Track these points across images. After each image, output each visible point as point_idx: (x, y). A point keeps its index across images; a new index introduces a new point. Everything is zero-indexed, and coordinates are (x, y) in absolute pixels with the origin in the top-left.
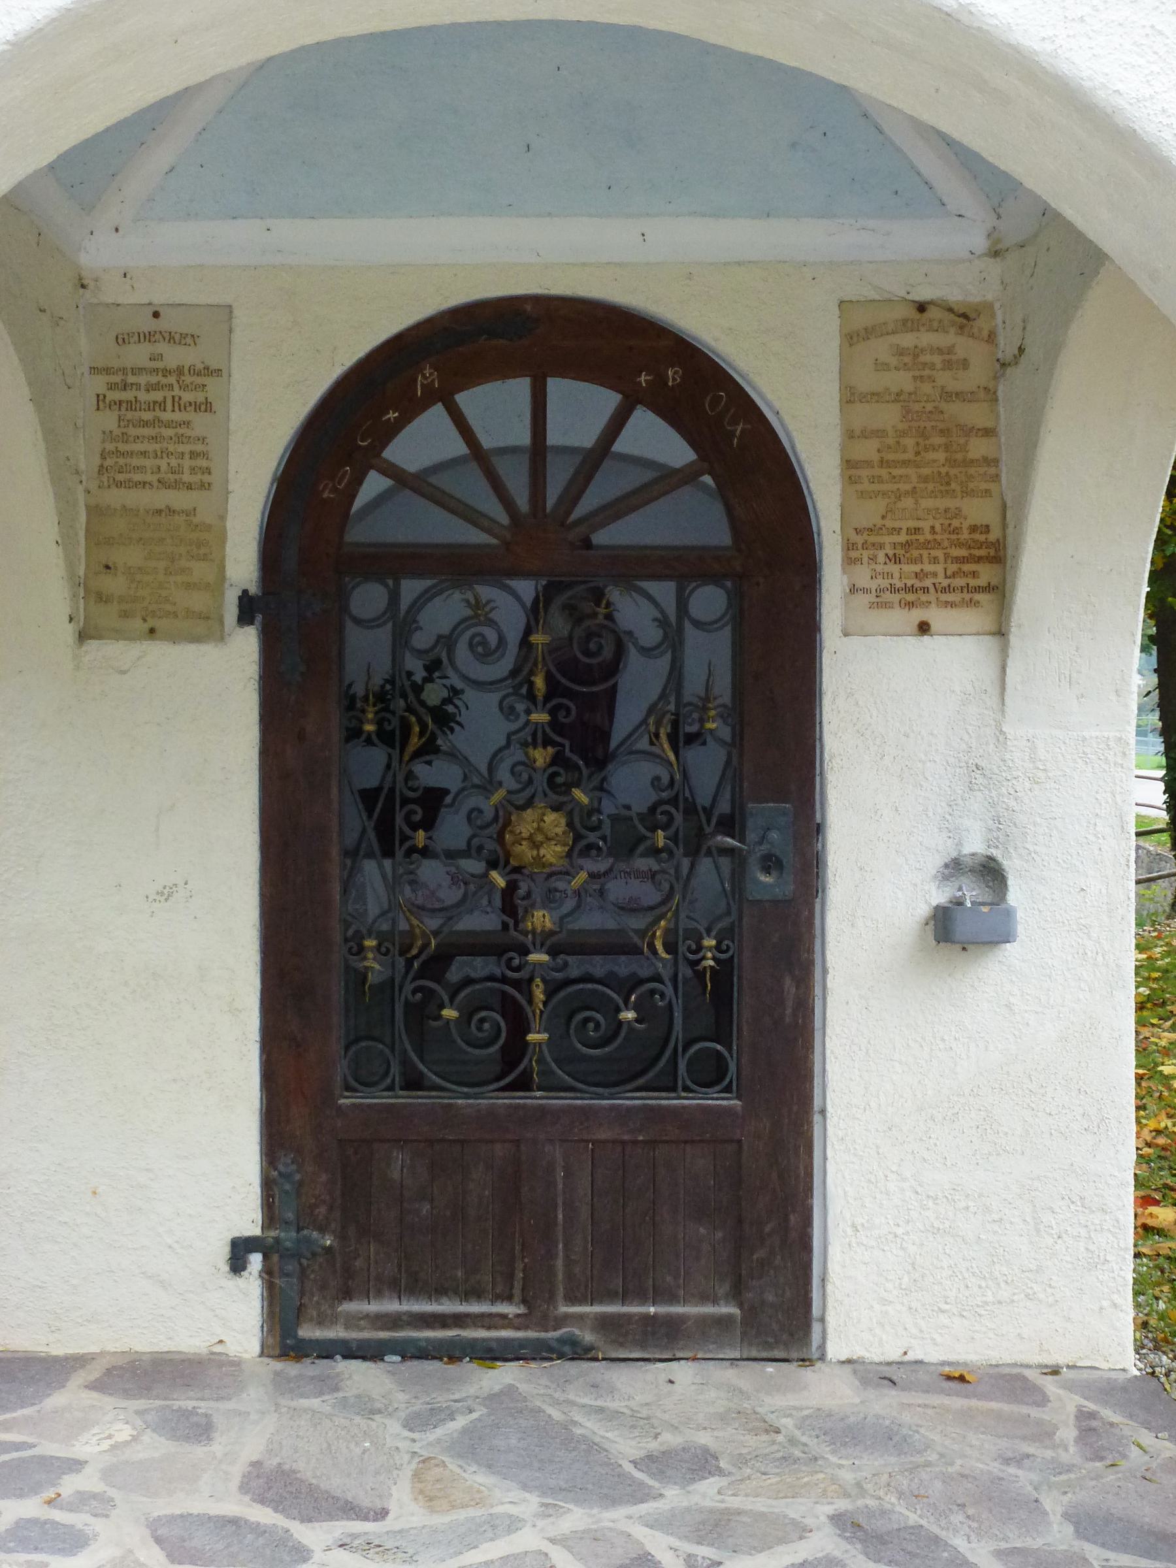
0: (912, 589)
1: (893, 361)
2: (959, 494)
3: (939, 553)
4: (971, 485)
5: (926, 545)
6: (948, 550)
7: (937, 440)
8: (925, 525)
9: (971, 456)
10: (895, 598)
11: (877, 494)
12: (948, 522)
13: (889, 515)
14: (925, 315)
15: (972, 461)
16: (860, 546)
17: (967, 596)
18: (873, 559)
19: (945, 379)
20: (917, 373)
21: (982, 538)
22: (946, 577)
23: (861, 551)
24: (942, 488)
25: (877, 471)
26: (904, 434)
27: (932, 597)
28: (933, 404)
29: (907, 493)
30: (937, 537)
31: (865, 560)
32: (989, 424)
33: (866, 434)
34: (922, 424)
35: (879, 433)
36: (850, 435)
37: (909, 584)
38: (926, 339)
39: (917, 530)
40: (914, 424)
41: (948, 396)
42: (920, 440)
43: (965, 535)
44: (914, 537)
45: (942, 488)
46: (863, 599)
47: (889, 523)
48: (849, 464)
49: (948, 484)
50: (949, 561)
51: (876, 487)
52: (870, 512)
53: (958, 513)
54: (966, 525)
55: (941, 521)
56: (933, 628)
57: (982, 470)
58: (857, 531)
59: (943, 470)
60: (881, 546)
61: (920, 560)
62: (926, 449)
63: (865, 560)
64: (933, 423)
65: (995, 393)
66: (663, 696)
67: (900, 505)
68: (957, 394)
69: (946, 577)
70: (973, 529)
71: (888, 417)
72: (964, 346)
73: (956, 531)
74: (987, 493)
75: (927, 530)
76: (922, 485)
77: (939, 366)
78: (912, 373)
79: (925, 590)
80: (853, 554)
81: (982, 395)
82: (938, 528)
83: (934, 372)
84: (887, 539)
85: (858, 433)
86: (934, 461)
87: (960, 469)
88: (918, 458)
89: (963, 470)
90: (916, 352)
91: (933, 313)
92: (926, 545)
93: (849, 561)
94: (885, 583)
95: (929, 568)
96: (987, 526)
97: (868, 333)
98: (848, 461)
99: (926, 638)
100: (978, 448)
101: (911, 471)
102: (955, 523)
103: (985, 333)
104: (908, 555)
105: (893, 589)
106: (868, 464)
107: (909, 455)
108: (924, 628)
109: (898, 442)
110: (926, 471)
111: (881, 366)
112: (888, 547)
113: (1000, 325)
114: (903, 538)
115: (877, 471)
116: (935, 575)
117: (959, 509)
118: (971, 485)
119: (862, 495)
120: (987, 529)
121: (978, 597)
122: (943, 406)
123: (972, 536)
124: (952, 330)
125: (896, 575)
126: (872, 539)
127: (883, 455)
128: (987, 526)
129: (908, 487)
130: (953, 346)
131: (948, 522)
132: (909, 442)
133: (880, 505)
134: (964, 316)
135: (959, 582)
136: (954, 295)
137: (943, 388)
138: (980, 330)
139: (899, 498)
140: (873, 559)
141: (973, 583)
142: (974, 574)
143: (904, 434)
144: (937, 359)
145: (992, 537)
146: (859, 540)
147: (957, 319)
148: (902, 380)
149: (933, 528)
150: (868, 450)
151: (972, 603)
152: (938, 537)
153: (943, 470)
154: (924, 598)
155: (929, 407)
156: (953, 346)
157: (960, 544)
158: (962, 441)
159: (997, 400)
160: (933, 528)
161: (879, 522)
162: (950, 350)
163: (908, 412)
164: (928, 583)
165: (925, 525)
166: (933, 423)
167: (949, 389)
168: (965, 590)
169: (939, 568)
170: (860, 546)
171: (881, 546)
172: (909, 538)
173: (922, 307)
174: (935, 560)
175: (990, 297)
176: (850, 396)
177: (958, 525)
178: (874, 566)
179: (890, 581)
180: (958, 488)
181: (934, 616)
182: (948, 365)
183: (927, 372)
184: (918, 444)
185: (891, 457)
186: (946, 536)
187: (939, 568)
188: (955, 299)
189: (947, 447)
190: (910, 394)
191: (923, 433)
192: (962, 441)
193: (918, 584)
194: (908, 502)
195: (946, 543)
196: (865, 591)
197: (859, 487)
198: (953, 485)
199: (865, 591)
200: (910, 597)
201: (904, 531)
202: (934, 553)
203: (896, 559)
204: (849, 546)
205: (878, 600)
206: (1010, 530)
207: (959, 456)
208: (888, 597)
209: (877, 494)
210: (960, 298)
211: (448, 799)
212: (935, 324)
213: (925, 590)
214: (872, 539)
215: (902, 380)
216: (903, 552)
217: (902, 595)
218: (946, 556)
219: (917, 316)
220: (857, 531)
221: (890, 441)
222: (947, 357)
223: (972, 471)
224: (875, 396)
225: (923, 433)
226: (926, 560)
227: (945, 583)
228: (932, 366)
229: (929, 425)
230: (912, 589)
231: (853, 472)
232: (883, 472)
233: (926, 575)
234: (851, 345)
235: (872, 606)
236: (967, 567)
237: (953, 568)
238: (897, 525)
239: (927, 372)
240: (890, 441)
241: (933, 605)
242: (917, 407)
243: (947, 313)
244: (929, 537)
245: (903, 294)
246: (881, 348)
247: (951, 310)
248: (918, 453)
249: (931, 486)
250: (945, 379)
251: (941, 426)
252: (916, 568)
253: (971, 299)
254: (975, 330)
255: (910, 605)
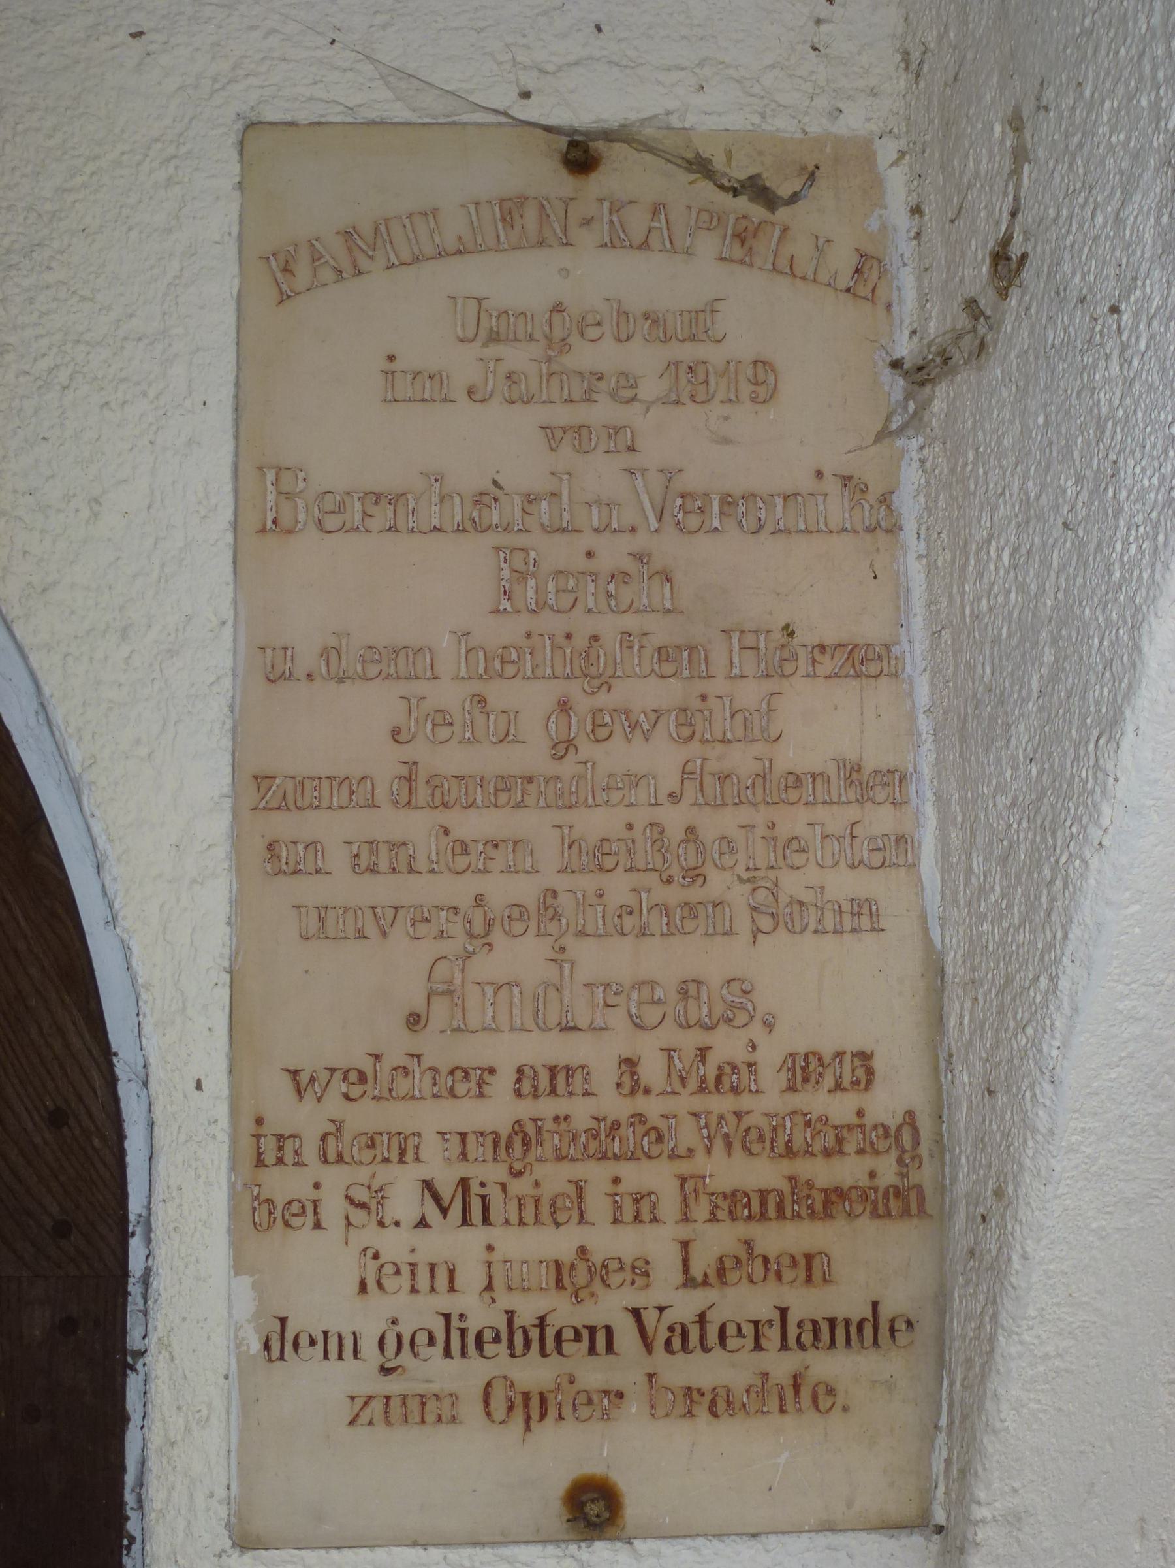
0: (542, 1338)
1: (464, 364)
2: (743, 924)
3: (657, 1177)
4: (792, 884)
5: (603, 1140)
6: (701, 1163)
7: (646, 693)
8: (599, 1056)
9: (788, 757)
10: (464, 1376)
11: (385, 920)
12: (690, 1041)
13: (440, 1007)
14: (598, 183)
15: (795, 780)
16: (310, 1153)
17: (781, 1365)
18: (367, 1205)
19: (681, 442)
20: (563, 415)
21: (841, 1108)
22: (689, 1283)
23: (315, 1169)
24: (673, 895)
25: (392, 824)
26: (501, 663)
27: (626, 1368)
28: (626, 543)
29: (519, 911)
30: (641, 1103)
31: (333, 1208)
32: (871, 630)
33: (341, 664)
34: (583, 625)
35: (396, 661)
36: (273, 668)
37: (527, 1310)
38: (599, 276)
39: (561, 1077)
40: (550, 623)
41: (686, 508)
42: (575, 690)
43: (769, 1099)
44: (547, 1107)
45: (673, 895)
46: (325, 1385)
47: (440, 1049)
48: (264, 791)
49: (695, 875)
50: (701, 1211)
51: (382, 890)
52: (349, 1003)
53: (740, 1004)
54: (770, 1055)
55: (669, 1035)
56: (633, 1510)
57: (836, 819)
58: (299, 1082)
59: (675, 819)
60: (404, 1148)
61: (573, 1206)
62: (599, 731)
63: (333, 1208)
64: (630, 622)
65: (885, 499)
66: (670, 390)
67: (486, 967)
68: (728, 502)
69: (689, 1283)
70: (804, 1069)
71: (441, 592)
72: (756, 311)
73: (730, 1079)
74: (863, 915)
75: (605, 1074)
76: (588, 883)
77: (649, 389)
78: (538, 414)
79: (597, 1340)
80: (286, 1184)
81: (836, 507)
82: (652, 1070)
83: (630, 414)
84: (431, 1118)
85: (307, 657)
86: (635, 780)
87: (745, 815)
88: (568, 768)
89: (760, 817)
90: (561, 327)
91: (622, 175)
92: (603, 1140)
93: (262, 1215)
94: (420, 1313)
95: (609, 1241)
96: (865, 1057)
97: (361, 249)
98: (262, 780)
99: (602, 1549)
100: (820, 725)
101: (536, 824)
102: (728, 1046)
103: (842, 261)
104: (519, 1187)
105: (457, 1338)
106: (352, 790)
107: (531, 756)
108: (593, 1508)
109: (481, 701)
110: (596, 823)
111: (410, 385)
112: (431, 1148)
113: (901, 220)
114: (499, 1110)
115: (392, 824)
116: (641, 1271)
117: (742, 989)
118: (792, 884)
119: (321, 924)
120: (863, 1068)
121: (825, 1365)
122: (669, 548)
123: (798, 1101)
124: (708, 245)
125: (471, 1276)
126: (363, 1117)
127: (418, 751)
128: (865, 1057)
129: (526, 890)
130: (711, 308)
131: (695, 1038)
132: (531, 700)
133: (405, 966)
134: (757, 190)
135: (749, 1302)
136: (714, 113)
137: (669, 474)
138: (822, 245)
139: (483, 938)
140: (367, 1205)
141: (806, 1303)
142: (811, 1268)
143: (501, 663)
144: (645, 359)
145: (885, 1104)
146: (307, 1119)
147: (726, 199)
148: (498, 445)
149: (630, 1064)
150: (348, 730)
151: (806, 1396)
152: (653, 1107)
153: (675, 819)
154: (594, 1374)
155: (614, 553)
156: (711, 308)
157: (743, 1139)
158: (750, 693)
159: (894, 530)
160: (630, 1064)
161: (397, 1045)
162: (699, 323)
163: (521, 576)
164: (610, 1307)
165: (599, 1056)
166: (630, 622)
167: (692, 480)
168: (772, 1335)
169: (658, 1244)
170: (310, 1153)
171: (404, 1148)
172: (525, 1109)
173: (580, 156)
174: (640, 1209)
175: (855, 121)
176: (276, 507)
177: (740, 1055)
178: (371, 1236)
179: (444, 1302)
180: (739, 895)
181: (639, 1452)
182: (692, 384)
183: (602, 412)
184: (564, 706)
185: (452, 759)
186: (686, 1102)
187: (658, 1244)
188: (712, 123)
189: (688, 723)
190: (530, 499)
191: (588, 663)
192: (750, 693)
193: (565, 1313)
194: (521, 957)
195: (688, 1135)
196: (334, 1346)
197: (311, 890)
198: (717, 883)
199: (334, 1346)
200: (534, 1372)
201: (503, 1083)
202: (636, 1176)
203: (468, 1205)
204: (262, 1148)
205: (393, 1386)
206: (965, 1081)
207: (741, 760)
208: (434, 1371)
209: (385, 920)
210: (738, 121)
211: (232, 1273)
212: (637, 222)
213: (597, 1340)
214: (363, 1117)
215: (498, 445)
216: (496, 1172)
217: (497, 1363)
218: (689, 1186)
219: (562, 183)
220: (299, 1082)
221: (449, 695)
222: (688, 352)
223: (795, 821)
224: (382, 508)
225: (588, 663)
226: (598, 1205)
227: (685, 1306)
228: (626, 388)
229: (609, 626)
230: (542, 1338)
231: (283, 825)
232: (416, 827)
233: (602, 1273)
234: (284, 298)
235: (361, 1411)
236: (777, 1238)
237: (717, 1240)
238: (473, 1051)
239: (602, 412)
240: (449, 695)
241: (634, 1407)
242: (560, 552)
243: (684, 177)
244: (615, 1106)
245: (504, 98)
246: (414, 312)
247: (701, 167)
248: (563, 747)
249: (619, 888)
250: (681, 442)
251: (662, 631)
252: (560, 1243)
253: (782, 124)
254: (801, 248)
255: (534, 1408)
